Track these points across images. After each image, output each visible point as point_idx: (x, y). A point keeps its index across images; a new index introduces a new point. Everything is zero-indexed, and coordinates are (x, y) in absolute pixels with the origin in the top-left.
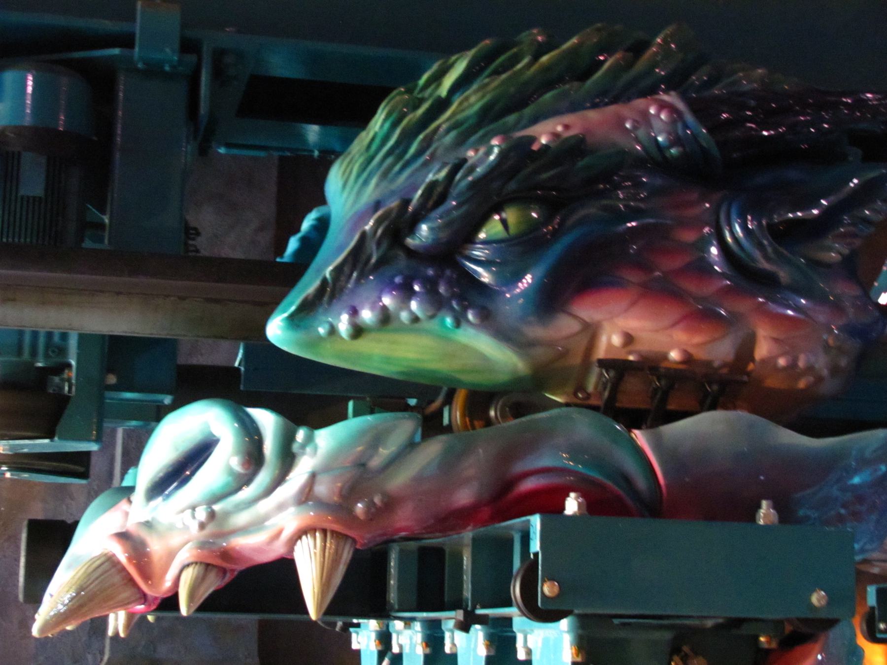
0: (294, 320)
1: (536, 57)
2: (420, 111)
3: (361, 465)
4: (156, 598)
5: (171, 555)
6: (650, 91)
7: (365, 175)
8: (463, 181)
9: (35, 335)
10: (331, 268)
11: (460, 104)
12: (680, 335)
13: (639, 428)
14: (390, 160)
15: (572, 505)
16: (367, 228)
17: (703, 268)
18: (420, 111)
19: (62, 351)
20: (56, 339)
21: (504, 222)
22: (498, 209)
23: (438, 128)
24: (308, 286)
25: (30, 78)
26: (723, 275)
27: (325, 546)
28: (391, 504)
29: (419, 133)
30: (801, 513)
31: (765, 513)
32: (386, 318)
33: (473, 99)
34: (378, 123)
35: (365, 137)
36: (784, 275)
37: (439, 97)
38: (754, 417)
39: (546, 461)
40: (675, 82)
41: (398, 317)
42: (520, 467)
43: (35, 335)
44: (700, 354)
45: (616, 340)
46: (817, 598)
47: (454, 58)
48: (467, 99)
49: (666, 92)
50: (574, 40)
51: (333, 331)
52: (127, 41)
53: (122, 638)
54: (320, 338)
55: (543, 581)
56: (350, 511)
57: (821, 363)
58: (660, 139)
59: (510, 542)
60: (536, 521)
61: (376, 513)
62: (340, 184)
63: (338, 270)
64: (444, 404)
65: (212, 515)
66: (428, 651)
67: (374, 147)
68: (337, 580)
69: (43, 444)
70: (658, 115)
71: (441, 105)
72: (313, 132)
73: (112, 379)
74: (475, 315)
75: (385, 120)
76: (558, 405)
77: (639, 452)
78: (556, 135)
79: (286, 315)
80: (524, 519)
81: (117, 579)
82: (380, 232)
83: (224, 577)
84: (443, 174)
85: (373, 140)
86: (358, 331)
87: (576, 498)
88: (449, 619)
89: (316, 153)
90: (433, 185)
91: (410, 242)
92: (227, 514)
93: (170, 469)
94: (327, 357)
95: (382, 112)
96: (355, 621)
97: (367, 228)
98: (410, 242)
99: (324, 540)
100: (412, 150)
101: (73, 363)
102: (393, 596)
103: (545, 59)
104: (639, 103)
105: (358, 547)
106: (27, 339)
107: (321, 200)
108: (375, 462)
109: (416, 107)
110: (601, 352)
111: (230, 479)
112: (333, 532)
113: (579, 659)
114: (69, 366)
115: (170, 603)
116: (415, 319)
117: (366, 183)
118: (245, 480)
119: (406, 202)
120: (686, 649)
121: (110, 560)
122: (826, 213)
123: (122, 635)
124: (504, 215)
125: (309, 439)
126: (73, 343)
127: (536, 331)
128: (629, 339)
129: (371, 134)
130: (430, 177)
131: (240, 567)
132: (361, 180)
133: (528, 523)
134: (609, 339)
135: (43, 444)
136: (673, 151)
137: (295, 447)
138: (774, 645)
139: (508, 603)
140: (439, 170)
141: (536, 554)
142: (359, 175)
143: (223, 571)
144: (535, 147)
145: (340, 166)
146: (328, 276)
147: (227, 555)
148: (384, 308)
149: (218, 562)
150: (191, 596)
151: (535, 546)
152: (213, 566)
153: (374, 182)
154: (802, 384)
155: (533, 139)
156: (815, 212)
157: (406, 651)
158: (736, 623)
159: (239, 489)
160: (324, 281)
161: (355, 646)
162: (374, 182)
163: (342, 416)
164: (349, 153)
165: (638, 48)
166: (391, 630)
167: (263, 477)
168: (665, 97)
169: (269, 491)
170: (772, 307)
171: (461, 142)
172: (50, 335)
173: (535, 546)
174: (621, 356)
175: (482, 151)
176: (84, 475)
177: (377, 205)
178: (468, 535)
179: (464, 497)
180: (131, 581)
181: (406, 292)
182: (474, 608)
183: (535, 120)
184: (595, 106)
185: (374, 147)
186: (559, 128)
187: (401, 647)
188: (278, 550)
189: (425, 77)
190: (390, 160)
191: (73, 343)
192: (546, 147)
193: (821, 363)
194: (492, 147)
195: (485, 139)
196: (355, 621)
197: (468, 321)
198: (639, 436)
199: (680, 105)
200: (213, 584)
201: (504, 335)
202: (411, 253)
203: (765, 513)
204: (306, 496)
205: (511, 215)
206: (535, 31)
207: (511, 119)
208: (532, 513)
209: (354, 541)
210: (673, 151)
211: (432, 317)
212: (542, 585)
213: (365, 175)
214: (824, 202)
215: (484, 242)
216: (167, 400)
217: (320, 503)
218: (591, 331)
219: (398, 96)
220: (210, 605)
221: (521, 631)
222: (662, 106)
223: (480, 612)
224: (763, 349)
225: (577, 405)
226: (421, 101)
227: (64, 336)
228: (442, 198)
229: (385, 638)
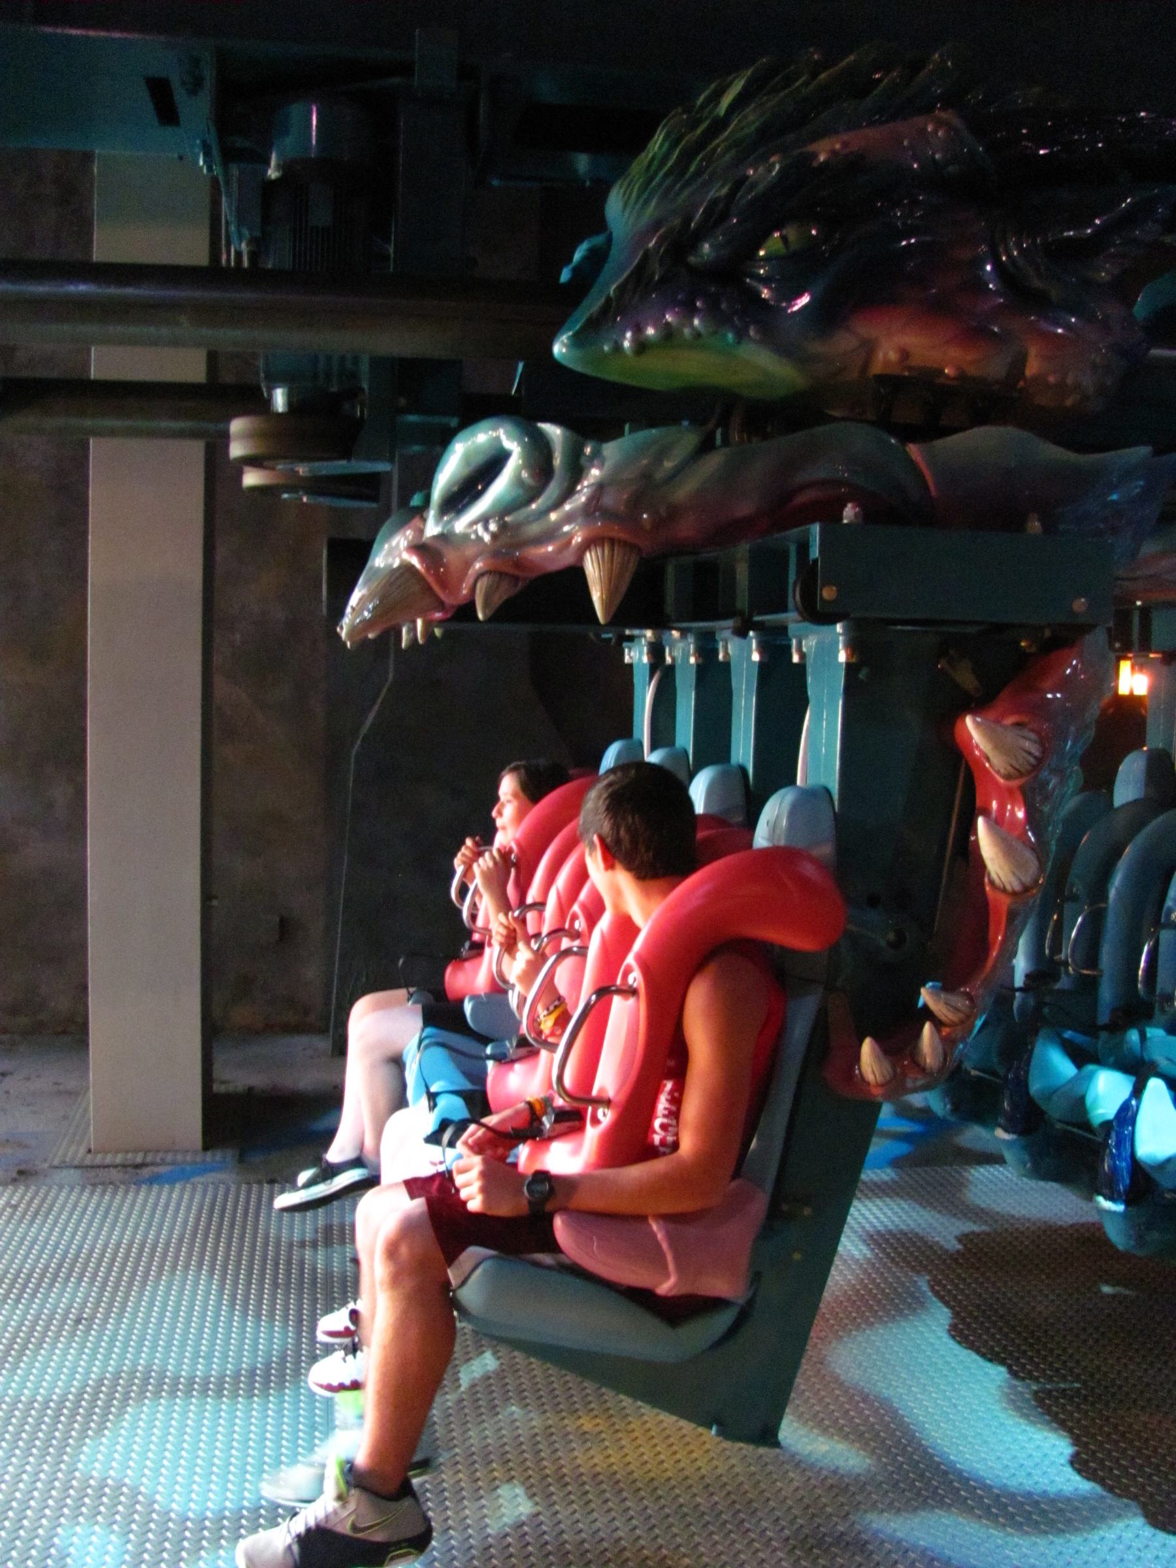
0: (578, 341)
1: (814, 75)
2: (699, 131)
3: (646, 476)
4: (453, 607)
5: (468, 564)
6: (928, 110)
7: (645, 196)
8: (746, 197)
9: (329, 358)
10: (614, 287)
11: (740, 121)
12: (954, 352)
13: (913, 441)
14: (668, 182)
15: (849, 513)
16: (651, 245)
17: (977, 286)
18: (699, 131)
19: (354, 376)
20: (349, 365)
21: (784, 239)
22: (778, 227)
23: (715, 149)
24: (592, 305)
25: (314, 109)
26: (996, 293)
27: (613, 555)
28: (674, 513)
29: (698, 153)
30: (1061, 527)
31: (1035, 526)
32: (669, 335)
33: (751, 118)
34: (657, 143)
35: (644, 158)
36: (1054, 294)
37: (718, 116)
38: (1025, 434)
39: (822, 474)
40: (952, 100)
41: (682, 333)
42: (801, 478)
43: (329, 358)
44: (972, 371)
45: (893, 356)
46: (1080, 604)
47: (730, 78)
48: (745, 117)
49: (943, 109)
50: (852, 58)
51: (618, 348)
52: (406, 69)
53: (420, 646)
54: (606, 356)
55: (823, 586)
56: (637, 519)
57: (1088, 382)
58: (937, 156)
59: (785, 554)
60: (816, 529)
61: (659, 523)
62: (621, 204)
63: (622, 289)
64: (717, 426)
65: (503, 527)
66: (700, 661)
67: (653, 168)
68: (624, 588)
69: (340, 466)
70: (935, 132)
71: (719, 125)
72: (582, 162)
73: (402, 402)
74: (757, 332)
75: (664, 140)
76: (835, 419)
77: (912, 464)
78: (834, 153)
79: (570, 333)
80: (803, 528)
81: (416, 588)
82: (662, 250)
83: (516, 585)
84: (725, 191)
85: (653, 159)
86: (642, 346)
87: (853, 508)
88: (724, 630)
89: (588, 184)
90: (714, 202)
91: (692, 259)
92: (517, 526)
93: (455, 489)
94: (612, 373)
95: (660, 133)
96: (627, 632)
97: (651, 245)
98: (692, 259)
99: (612, 550)
100: (692, 169)
101: (365, 386)
102: (670, 608)
103: (823, 76)
104: (919, 120)
105: (644, 555)
106: (321, 365)
107: (599, 224)
108: (659, 475)
109: (694, 127)
110: (877, 368)
111: (521, 492)
112: (619, 541)
113: (854, 660)
114: (363, 390)
115: (467, 610)
116: (698, 335)
117: (647, 202)
118: (533, 494)
119: (688, 220)
120: (952, 652)
121: (407, 568)
122: (1100, 232)
123: (420, 641)
124: (784, 232)
125: (596, 454)
126: (365, 367)
127: (816, 347)
128: (905, 354)
129: (650, 155)
130: (712, 194)
131: (533, 575)
132: (641, 201)
133: (808, 532)
134: (885, 355)
135: (340, 466)
136: (951, 169)
137: (583, 461)
138: (1033, 650)
139: (784, 609)
140: (723, 186)
141: (815, 561)
142: (638, 197)
143: (516, 579)
144: (815, 164)
145: (621, 188)
146: (612, 293)
147: (519, 564)
148: (667, 324)
149: (511, 571)
150: (486, 604)
151: (815, 552)
152: (506, 574)
153: (653, 203)
154: (1069, 402)
155: (815, 155)
156: (1097, 222)
157: (679, 661)
158: (999, 628)
159: (532, 499)
160: (609, 300)
161: (627, 660)
162: (653, 203)
163: (621, 434)
164: (629, 174)
165: (915, 67)
166: (664, 642)
167: (553, 489)
168: (944, 115)
169: (557, 505)
170: (1044, 326)
171: (739, 161)
172: (342, 359)
173: (815, 552)
174: (897, 371)
175: (761, 170)
176: (373, 498)
177: (656, 225)
178: (743, 549)
179: (744, 508)
180: (429, 588)
181: (690, 310)
182: (751, 616)
183: (816, 137)
184: (871, 124)
185: (653, 168)
186: (838, 146)
187: (673, 659)
188: (568, 559)
189: (702, 98)
190: (668, 182)
191: (365, 367)
192: (826, 162)
193: (1088, 382)
194: (773, 165)
195: (764, 158)
196: (627, 632)
197: (749, 336)
198: (913, 450)
199: (956, 122)
200: (504, 593)
201: (785, 350)
202: (693, 270)
203: (1035, 526)
204: (592, 509)
205: (791, 232)
206: (812, 49)
207: (790, 137)
208: (813, 521)
209: (640, 550)
210: (951, 169)
211: (715, 333)
212: (821, 590)
213: (645, 196)
214: (1097, 222)
215: (766, 259)
216: (454, 422)
217: (609, 515)
218: (869, 347)
219: (678, 116)
220: (501, 614)
221: (795, 637)
222: (939, 123)
223: (757, 618)
224: (1033, 367)
225: (853, 420)
226: (699, 121)
227: (356, 360)
228: (724, 216)
229: (656, 651)
